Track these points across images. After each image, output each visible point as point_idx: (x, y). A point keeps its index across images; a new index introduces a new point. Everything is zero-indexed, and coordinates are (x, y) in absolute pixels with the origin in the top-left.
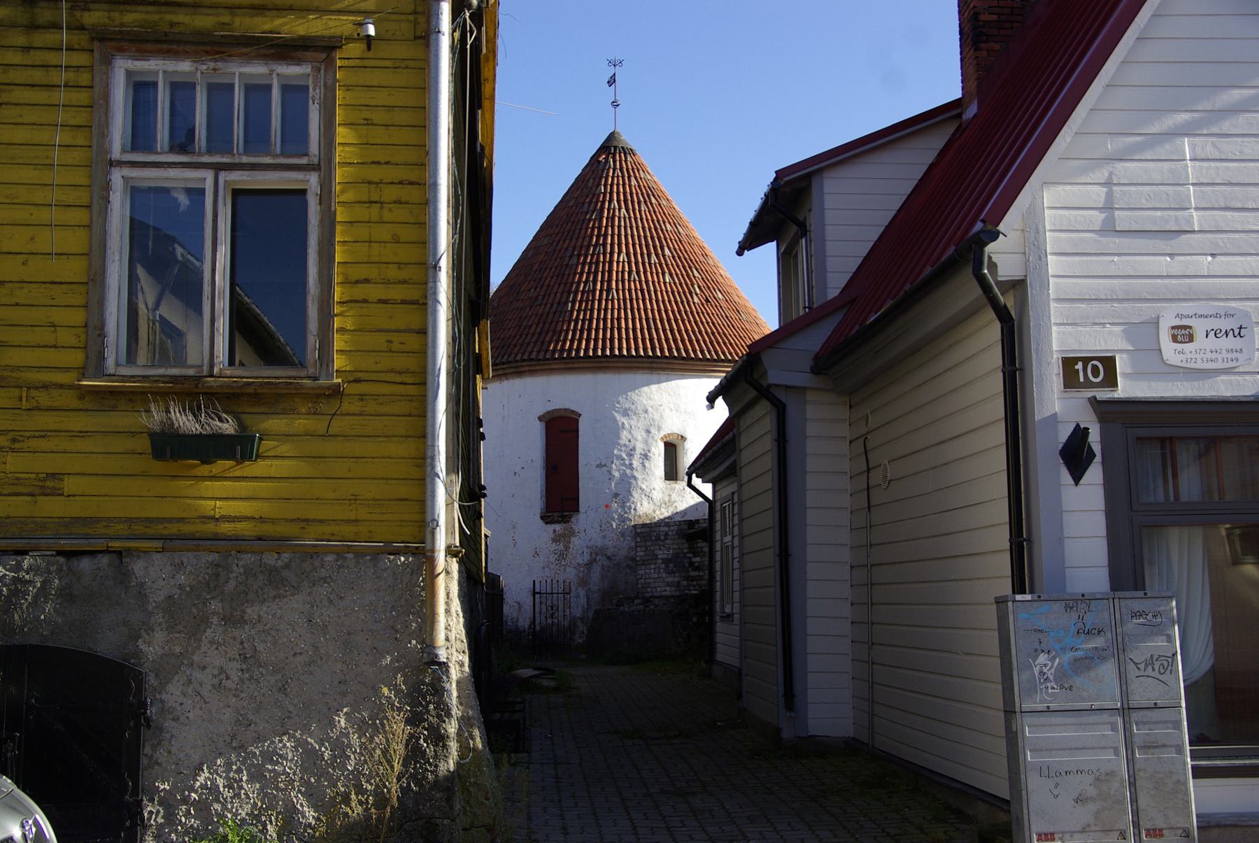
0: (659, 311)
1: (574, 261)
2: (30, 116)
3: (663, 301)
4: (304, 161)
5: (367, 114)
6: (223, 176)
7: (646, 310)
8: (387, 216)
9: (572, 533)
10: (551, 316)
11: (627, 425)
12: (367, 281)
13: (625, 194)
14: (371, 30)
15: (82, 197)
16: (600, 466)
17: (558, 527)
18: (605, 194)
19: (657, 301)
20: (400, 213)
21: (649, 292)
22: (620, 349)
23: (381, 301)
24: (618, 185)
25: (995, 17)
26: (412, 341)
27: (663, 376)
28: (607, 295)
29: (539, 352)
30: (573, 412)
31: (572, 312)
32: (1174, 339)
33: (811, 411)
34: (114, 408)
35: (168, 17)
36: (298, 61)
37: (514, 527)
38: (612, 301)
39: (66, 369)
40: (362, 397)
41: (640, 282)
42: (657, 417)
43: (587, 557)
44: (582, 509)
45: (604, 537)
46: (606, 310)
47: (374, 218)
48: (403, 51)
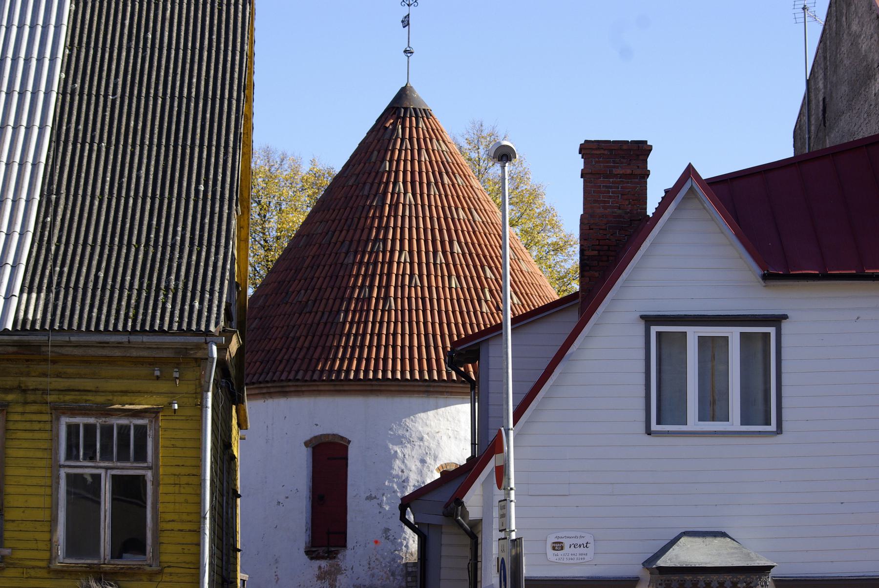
0: (441, 324)
1: (350, 260)
2: (25, 444)
3: (447, 312)
4: (145, 465)
5: (173, 442)
6: (109, 471)
7: (425, 323)
8: (182, 491)
10: (321, 327)
11: (400, 454)
12: (173, 521)
13: (413, 172)
14: (176, 407)
15: (48, 482)
16: (370, 498)
17: (323, 563)
18: (389, 172)
19: (439, 312)
20: (189, 490)
21: (431, 300)
22: (394, 372)
23: (180, 530)
24: (405, 161)
25: (596, 253)
26: (193, 549)
27: (441, 400)
28: (384, 306)
29: (306, 371)
30: (342, 438)
31: (344, 323)
32: (554, 548)
33: (445, 539)
34: (63, 578)
35: (85, 397)
36: (143, 418)
37: (277, 561)
38: (389, 311)
39: (42, 560)
40: (171, 574)
41: (422, 288)
42: (433, 445)
44: (350, 543)
45: (373, 575)
46: (381, 323)
47: (177, 491)
48: (189, 412)
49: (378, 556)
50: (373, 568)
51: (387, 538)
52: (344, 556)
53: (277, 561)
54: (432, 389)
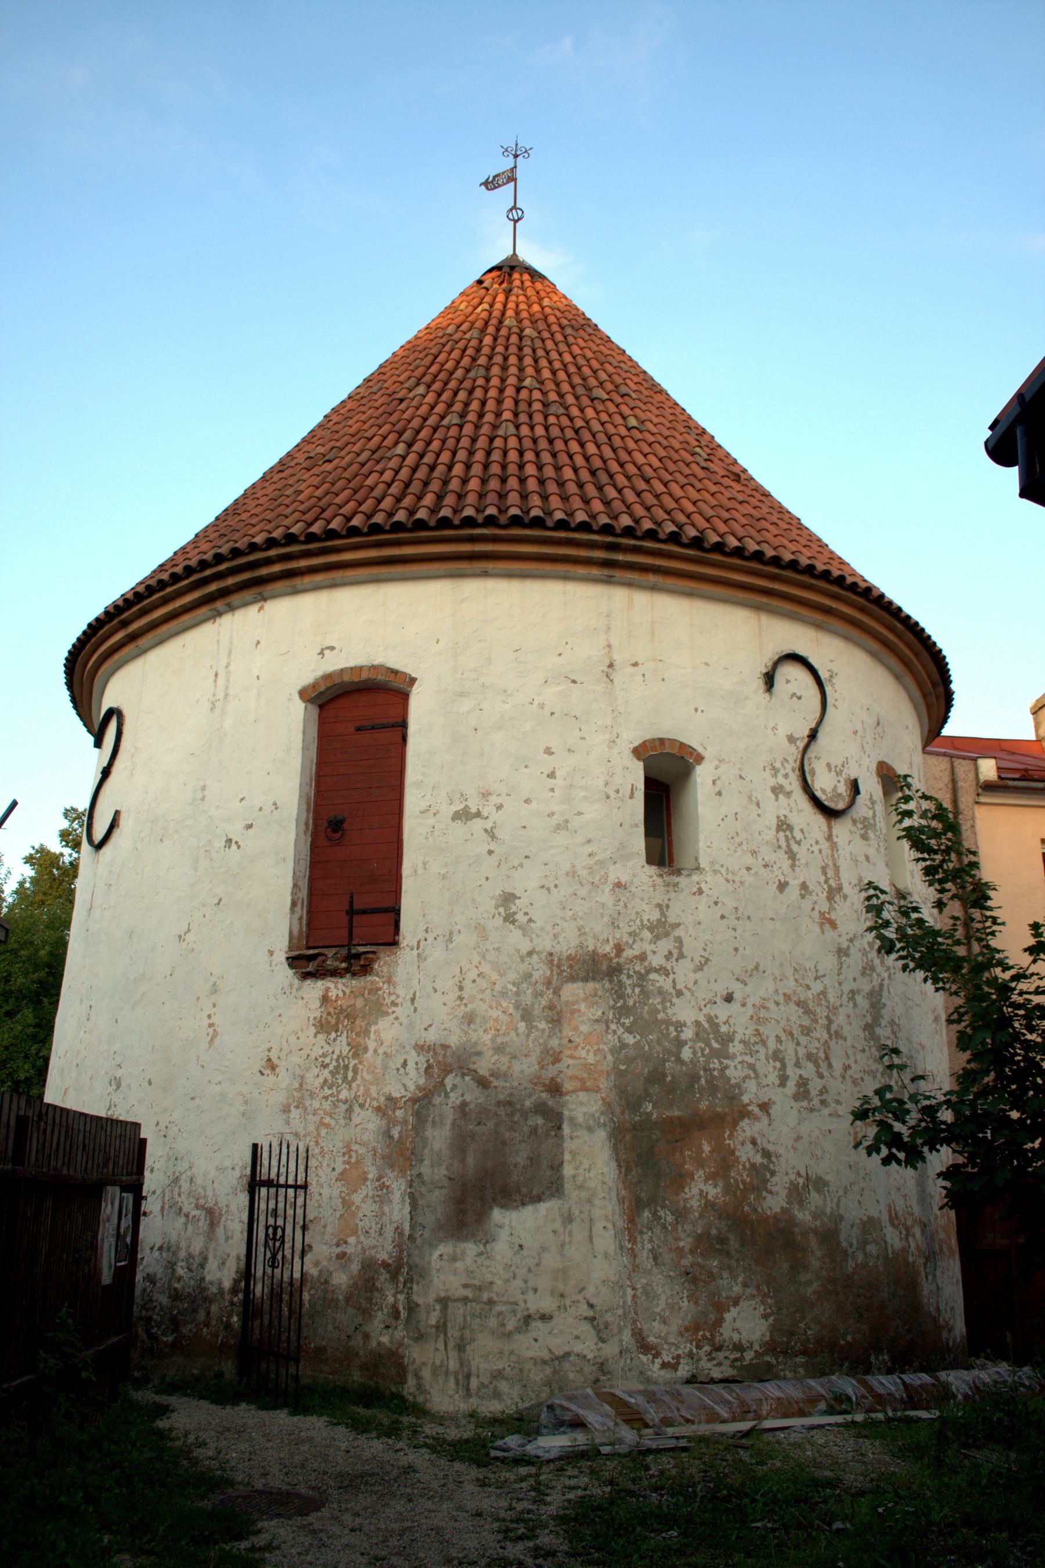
9: (378, 1009)
16: (464, 815)
17: (336, 988)
30: (395, 672)
37: (215, 990)
43: (414, 1079)
45: (470, 1019)
49: (486, 968)
50: (472, 999)
51: (510, 918)
52: (766, 666)
53: (215, 990)
54: (620, 557)
